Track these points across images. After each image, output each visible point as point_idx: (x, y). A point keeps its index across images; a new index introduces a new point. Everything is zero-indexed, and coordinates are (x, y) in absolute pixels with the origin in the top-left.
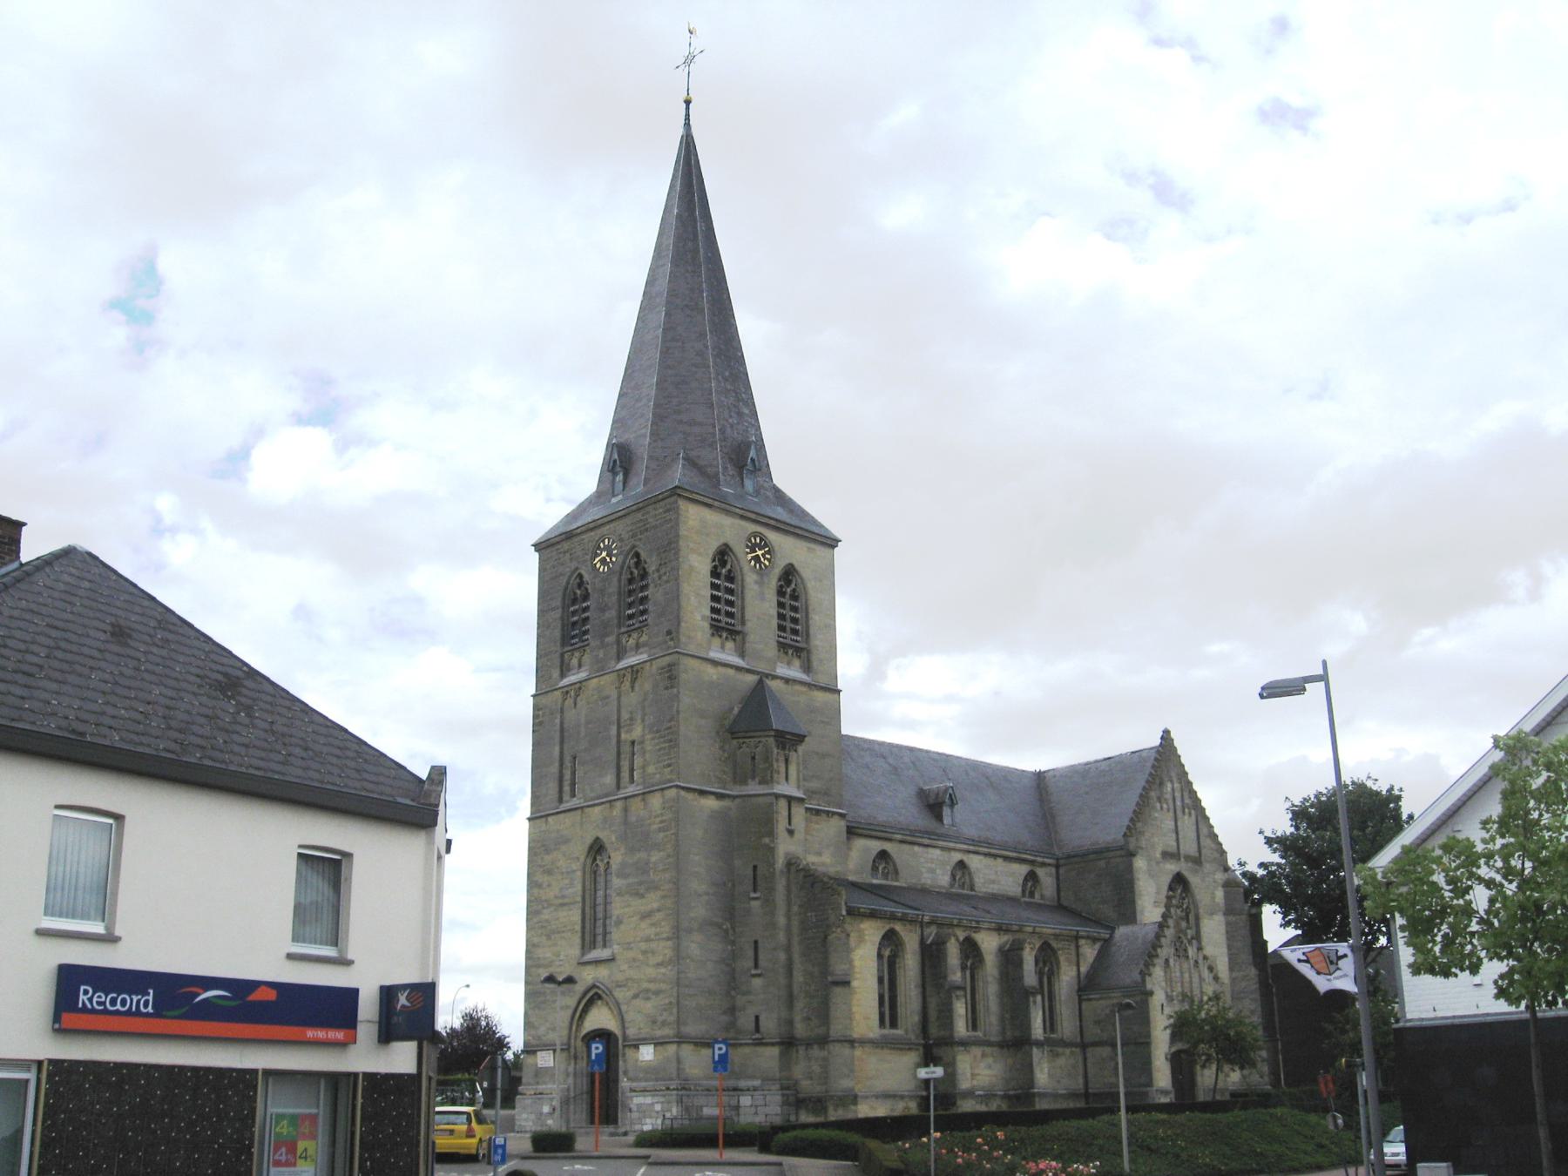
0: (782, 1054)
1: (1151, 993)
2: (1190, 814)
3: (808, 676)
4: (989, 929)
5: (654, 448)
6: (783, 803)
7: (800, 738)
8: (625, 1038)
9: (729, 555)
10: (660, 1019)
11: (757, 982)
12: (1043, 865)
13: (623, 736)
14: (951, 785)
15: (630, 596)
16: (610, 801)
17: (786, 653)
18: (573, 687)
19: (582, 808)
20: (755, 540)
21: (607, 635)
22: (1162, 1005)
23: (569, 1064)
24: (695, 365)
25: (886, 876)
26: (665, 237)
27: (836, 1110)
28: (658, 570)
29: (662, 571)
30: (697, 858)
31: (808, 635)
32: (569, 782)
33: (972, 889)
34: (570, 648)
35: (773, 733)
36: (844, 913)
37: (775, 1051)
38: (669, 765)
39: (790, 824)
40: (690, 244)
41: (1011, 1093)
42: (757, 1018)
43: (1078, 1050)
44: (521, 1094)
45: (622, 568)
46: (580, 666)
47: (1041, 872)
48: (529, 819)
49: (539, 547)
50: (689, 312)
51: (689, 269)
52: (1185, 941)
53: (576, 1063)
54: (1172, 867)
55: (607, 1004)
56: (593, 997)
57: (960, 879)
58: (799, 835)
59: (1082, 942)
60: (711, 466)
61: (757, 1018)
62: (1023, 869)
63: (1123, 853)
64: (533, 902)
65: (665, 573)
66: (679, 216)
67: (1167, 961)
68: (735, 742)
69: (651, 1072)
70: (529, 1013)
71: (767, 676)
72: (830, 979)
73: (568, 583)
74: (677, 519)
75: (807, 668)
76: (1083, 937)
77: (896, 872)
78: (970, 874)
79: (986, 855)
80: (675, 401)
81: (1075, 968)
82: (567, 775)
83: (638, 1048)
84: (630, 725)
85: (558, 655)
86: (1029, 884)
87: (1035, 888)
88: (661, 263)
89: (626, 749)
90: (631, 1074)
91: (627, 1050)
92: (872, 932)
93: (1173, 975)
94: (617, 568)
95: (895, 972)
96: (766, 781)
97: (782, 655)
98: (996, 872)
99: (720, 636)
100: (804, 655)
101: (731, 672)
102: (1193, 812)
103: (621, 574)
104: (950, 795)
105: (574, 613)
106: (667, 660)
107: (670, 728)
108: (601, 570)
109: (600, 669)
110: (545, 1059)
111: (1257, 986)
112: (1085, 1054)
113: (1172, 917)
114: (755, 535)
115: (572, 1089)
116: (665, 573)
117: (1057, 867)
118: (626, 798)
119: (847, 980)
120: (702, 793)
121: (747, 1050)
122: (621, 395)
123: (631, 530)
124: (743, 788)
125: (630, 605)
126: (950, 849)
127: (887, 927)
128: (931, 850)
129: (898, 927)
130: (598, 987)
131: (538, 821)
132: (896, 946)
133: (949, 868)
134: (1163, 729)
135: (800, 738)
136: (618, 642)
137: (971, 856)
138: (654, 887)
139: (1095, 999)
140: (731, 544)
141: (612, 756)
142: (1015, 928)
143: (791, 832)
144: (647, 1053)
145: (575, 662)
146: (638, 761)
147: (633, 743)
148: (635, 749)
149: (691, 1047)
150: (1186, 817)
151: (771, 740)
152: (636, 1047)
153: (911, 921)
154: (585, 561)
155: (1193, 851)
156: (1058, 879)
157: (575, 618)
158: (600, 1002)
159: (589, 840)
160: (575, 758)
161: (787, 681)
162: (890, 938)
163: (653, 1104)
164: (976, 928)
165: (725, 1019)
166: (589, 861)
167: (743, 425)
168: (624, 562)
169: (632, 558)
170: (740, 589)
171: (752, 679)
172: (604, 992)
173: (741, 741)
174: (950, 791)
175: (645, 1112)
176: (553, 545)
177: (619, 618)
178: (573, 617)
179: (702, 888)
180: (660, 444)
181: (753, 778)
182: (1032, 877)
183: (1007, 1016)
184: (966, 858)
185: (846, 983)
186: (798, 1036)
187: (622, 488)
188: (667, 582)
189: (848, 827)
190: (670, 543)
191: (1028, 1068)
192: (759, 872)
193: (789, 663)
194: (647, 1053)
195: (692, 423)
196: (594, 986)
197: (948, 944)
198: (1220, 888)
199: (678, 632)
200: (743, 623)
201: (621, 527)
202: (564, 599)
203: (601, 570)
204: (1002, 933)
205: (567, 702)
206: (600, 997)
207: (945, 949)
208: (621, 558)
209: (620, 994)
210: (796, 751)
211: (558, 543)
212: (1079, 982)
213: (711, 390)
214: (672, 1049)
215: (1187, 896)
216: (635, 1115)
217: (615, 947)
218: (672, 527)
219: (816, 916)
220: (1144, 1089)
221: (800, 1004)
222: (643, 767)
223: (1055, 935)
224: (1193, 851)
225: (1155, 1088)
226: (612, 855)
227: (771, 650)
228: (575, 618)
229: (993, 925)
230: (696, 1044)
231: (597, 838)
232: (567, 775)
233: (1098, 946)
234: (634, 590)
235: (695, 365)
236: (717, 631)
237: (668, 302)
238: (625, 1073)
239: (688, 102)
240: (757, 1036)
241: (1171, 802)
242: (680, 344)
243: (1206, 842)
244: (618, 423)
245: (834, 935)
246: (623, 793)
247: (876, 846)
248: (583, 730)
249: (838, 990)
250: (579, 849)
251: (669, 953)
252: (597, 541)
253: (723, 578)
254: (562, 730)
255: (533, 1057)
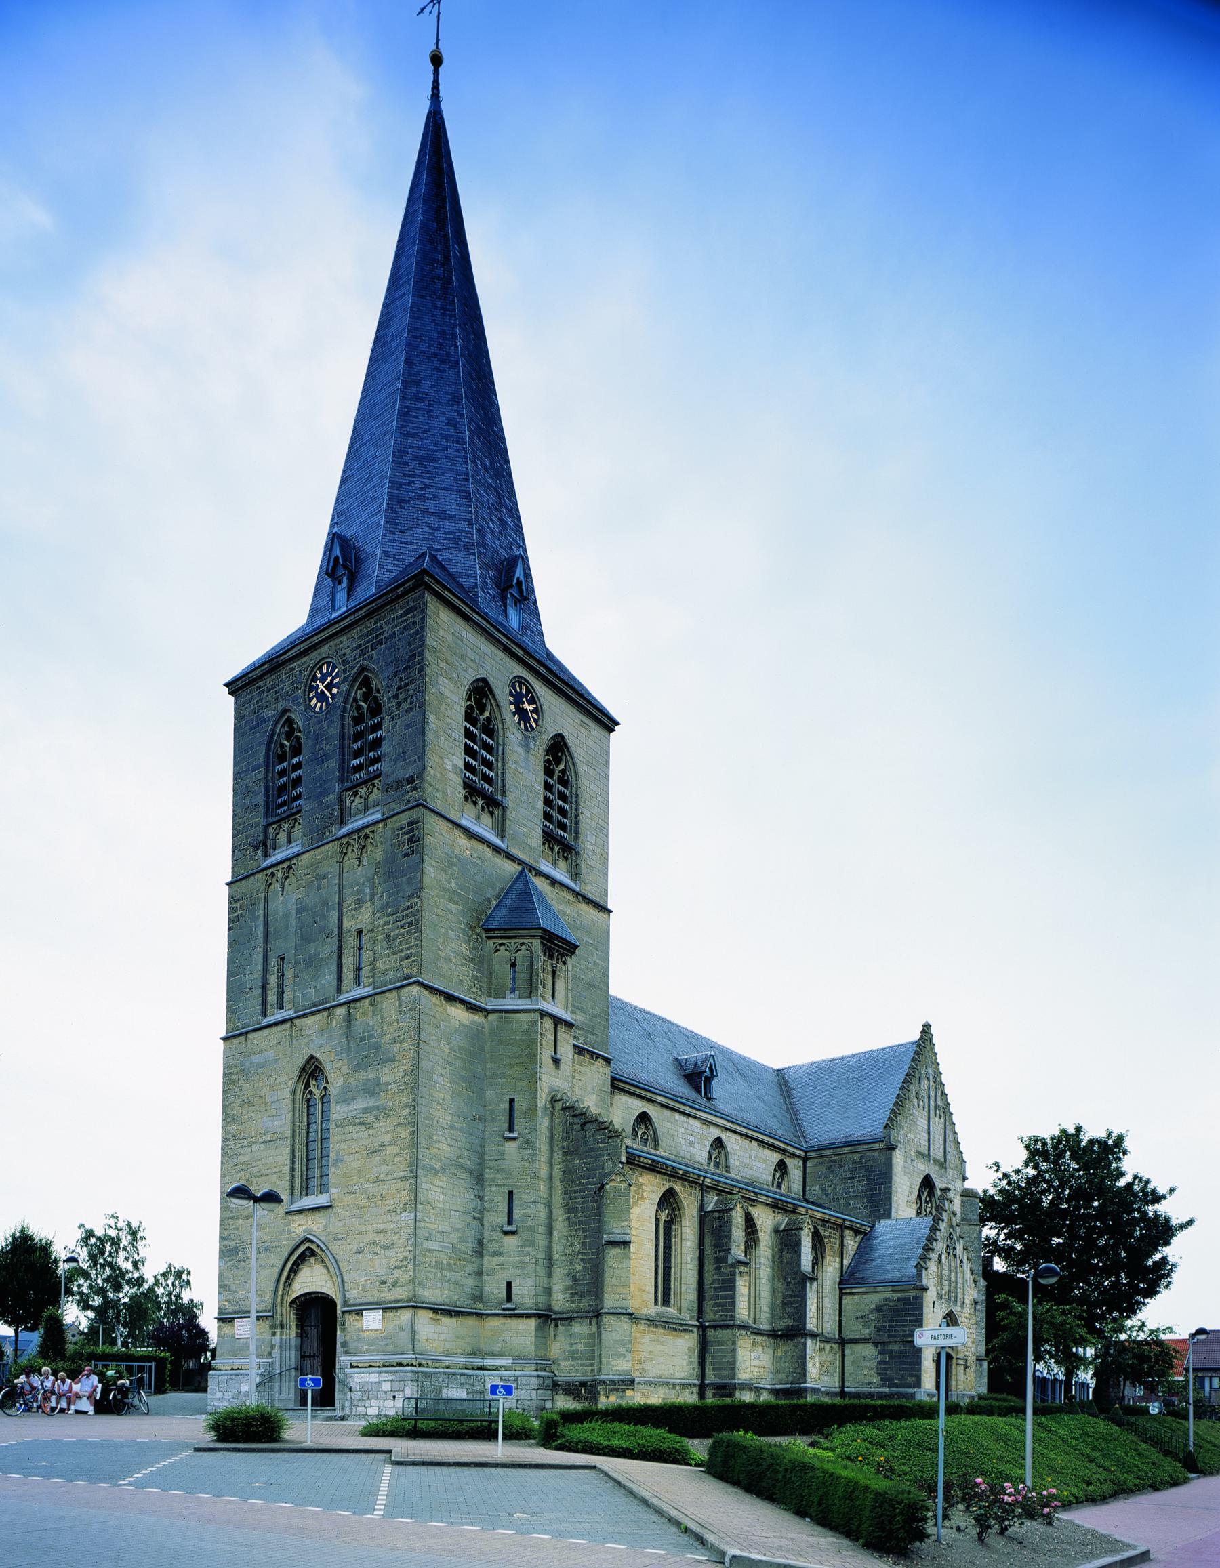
0: (539, 1329)
1: (925, 1289)
2: (940, 1116)
3: (576, 884)
4: (766, 1204)
5: (390, 541)
6: (548, 1024)
7: (571, 948)
8: (346, 1303)
9: (488, 698)
10: (390, 1279)
11: (511, 1241)
12: (793, 1155)
13: (346, 925)
14: (713, 1054)
15: (355, 741)
16: (328, 1009)
17: (552, 849)
18: (281, 866)
19: (291, 1020)
20: (521, 689)
21: (324, 793)
22: (934, 1303)
23: (274, 1334)
24: (445, 437)
25: (645, 1142)
26: (404, 259)
27: (607, 1397)
28: (396, 697)
29: (401, 697)
30: (441, 1080)
31: (577, 831)
32: (275, 991)
33: (728, 1169)
34: (277, 818)
35: (539, 933)
36: (624, 1160)
37: (532, 1324)
38: (408, 957)
39: (555, 1053)
40: (440, 271)
41: (778, 1387)
42: (509, 1284)
43: (835, 1346)
44: (214, 1369)
45: (346, 701)
46: (289, 841)
47: (790, 1162)
48: (224, 1039)
49: (236, 686)
50: (437, 363)
51: (439, 304)
52: (955, 1238)
53: (281, 1334)
54: (923, 1168)
55: (323, 1261)
56: (304, 1254)
57: (716, 1158)
58: (566, 1067)
59: (846, 1232)
60: (467, 575)
61: (509, 1284)
62: (776, 1157)
63: (882, 1145)
64: (229, 1139)
65: (406, 699)
66: (423, 227)
67: (940, 1256)
68: (490, 942)
69: (375, 1342)
70: (226, 1273)
71: (531, 868)
72: (606, 1237)
73: (273, 732)
74: (423, 620)
75: (575, 874)
76: (847, 1228)
77: (656, 1139)
78: (726, 1153)
79: (742, 1135)
80: (418, 482)
81: (838, 1260)
82: (273, 980)
83: (362, 1314)
84: (356, 909)
85: (260, 828)
86: (778, 1175)
87: (783, 1179)
88: (399, 293)
89: (350, 942)
90: (351, 1347)
91: (347, 1317)
92: (650, 1188)
93: (944, 1272)
94: (340, 701)
95: (670, 1240)
96: (531, 991)
97: (548, 851)
98: (750, 1157)
99: (475, 803)
100: (572, 857)
101: (488, 852)
102: (942, 1115)
103: (344, 710)
104: (711, 1065)
105: (282, 773)
106: (405, 818)
107: (408, 908)
108: (317, 709)
109: (316, 840)
110: (244, 1328)
111: (984, 1298)
112: (843, 1351)
113: (946, 1211)
114: (521, 681)
115: (277, 1363)
116: (406, 699)
117: (805, 1160)
118: (349, 1002)
119: (628, 1239)
120: (450, 998)
121: (495, 1323)
122: (344, 481)
123: (360, 646)
124: (500, 1001)
125: (357, 754)
126: (708, 1123)
127: (667, 1186)
128: (691, 1121)
129: (678, 1187)
130: (312, 1242)
131: (235, 1041)
132: (673, 1210)
133: (706, 1143)
134: (923, 1023)
135: (571, 948)
136: (341, 801)
137: (729, 1134)
138: (382, 1112)
139: (859, 1293)
140: (491, 680)
141: (330, 948)
142: (790, 1207)
143: (556, 1062)
144: (373, 1320)
145: (282, 837)
146: (367, 956)
147: (360, 933)
148: (363, 942)
149: (430, 1314)
150: (937, 1119)
151: (537, 945)
152: (359, 1313)
153: (692, 1182)
154: (296, 698)
155: (940, 1157)
156: (804, 1172)
157: (284, 780)
158: (313, 1260)
159: (301, 1061)
160: (283, 959)
161: (554, 882)
162: (668, 1200)
163: (379, 1383)
164: (753, 1200)
165: (471, 1283)
166: (301, 1086)
167: (506, 539)
168: (348, 694)
169: (359, 688)
170: (500, 748)
171: (512, 869)
172: (318, 1246)
173: (500, 941)
174: (711, 1060)
175: (369, 1393)
176: (252, 682)
177: (342, 770)
178: (280, 778)
179: (447, 1119)
180: (398, 537)
181: (513, 990)
182: (781, 1167)
183: (778, 1302)
184: (726, 1137)
185: (625, 1244)
186: (557, 1308)
187: (345, 598)
188: (409, 710)
189: (613, 1079)
190: (412, 657)
191: (801, 1361)
192: (517, 1106)
193: (554, 863)
194: (373, 1320)
195: (442, 515)
196: (306, 1240)
197: (734, 1213)
198: (958, 1197)
199: (422, 778)
200: (503, 793)
201: (346, 645)
202: (267, 756)
203: (317, 709)
204: (777, 1211)
205: (272, 889)
206: (313, 1254)
207: (730, 1217)
208: (345, 687)
209: (342, 1251)
210: (565, 963)
211: (261, 677)
212: (842, 1275)
213: (467, 475)
214: (405, 1316)
215: (930, 1200)
216: (356, 1396)
217: (333, 1190)
218: (416, 633)
219: (585, 1164)
220: (910, 1391)
221: (560, 1271)
222: (372, 963)
223: (823, 1221)
224: (940, 1157)
225: (923, 1390)
226: (330, 1077)
227: (536, 840)
228: (284, 780)
229: (770, 1200)
230: (434, 1310)
231: (312, 1057)
232: (273, 980)
233: (858, 1239)
234: (362, 731)
235: (445, 437)
236: (472, 795)
237: (409, 345)
238: (344, 1344)
239: (437, 60)
240: (509, 1306)
241: (926, 1100)
242: (424, 406)
243: (951, 1148)
244: (340, 514)
245: (612, 1184)
246: (344, 997)
247: (639, 1106)
248: (293, 922)
249: (615, 1251)
250: (288, 1075)
251: (405, 1197)
252: (313, 669)
253: (479, 725)
254: (266, 924)
255: (228, 1325)
